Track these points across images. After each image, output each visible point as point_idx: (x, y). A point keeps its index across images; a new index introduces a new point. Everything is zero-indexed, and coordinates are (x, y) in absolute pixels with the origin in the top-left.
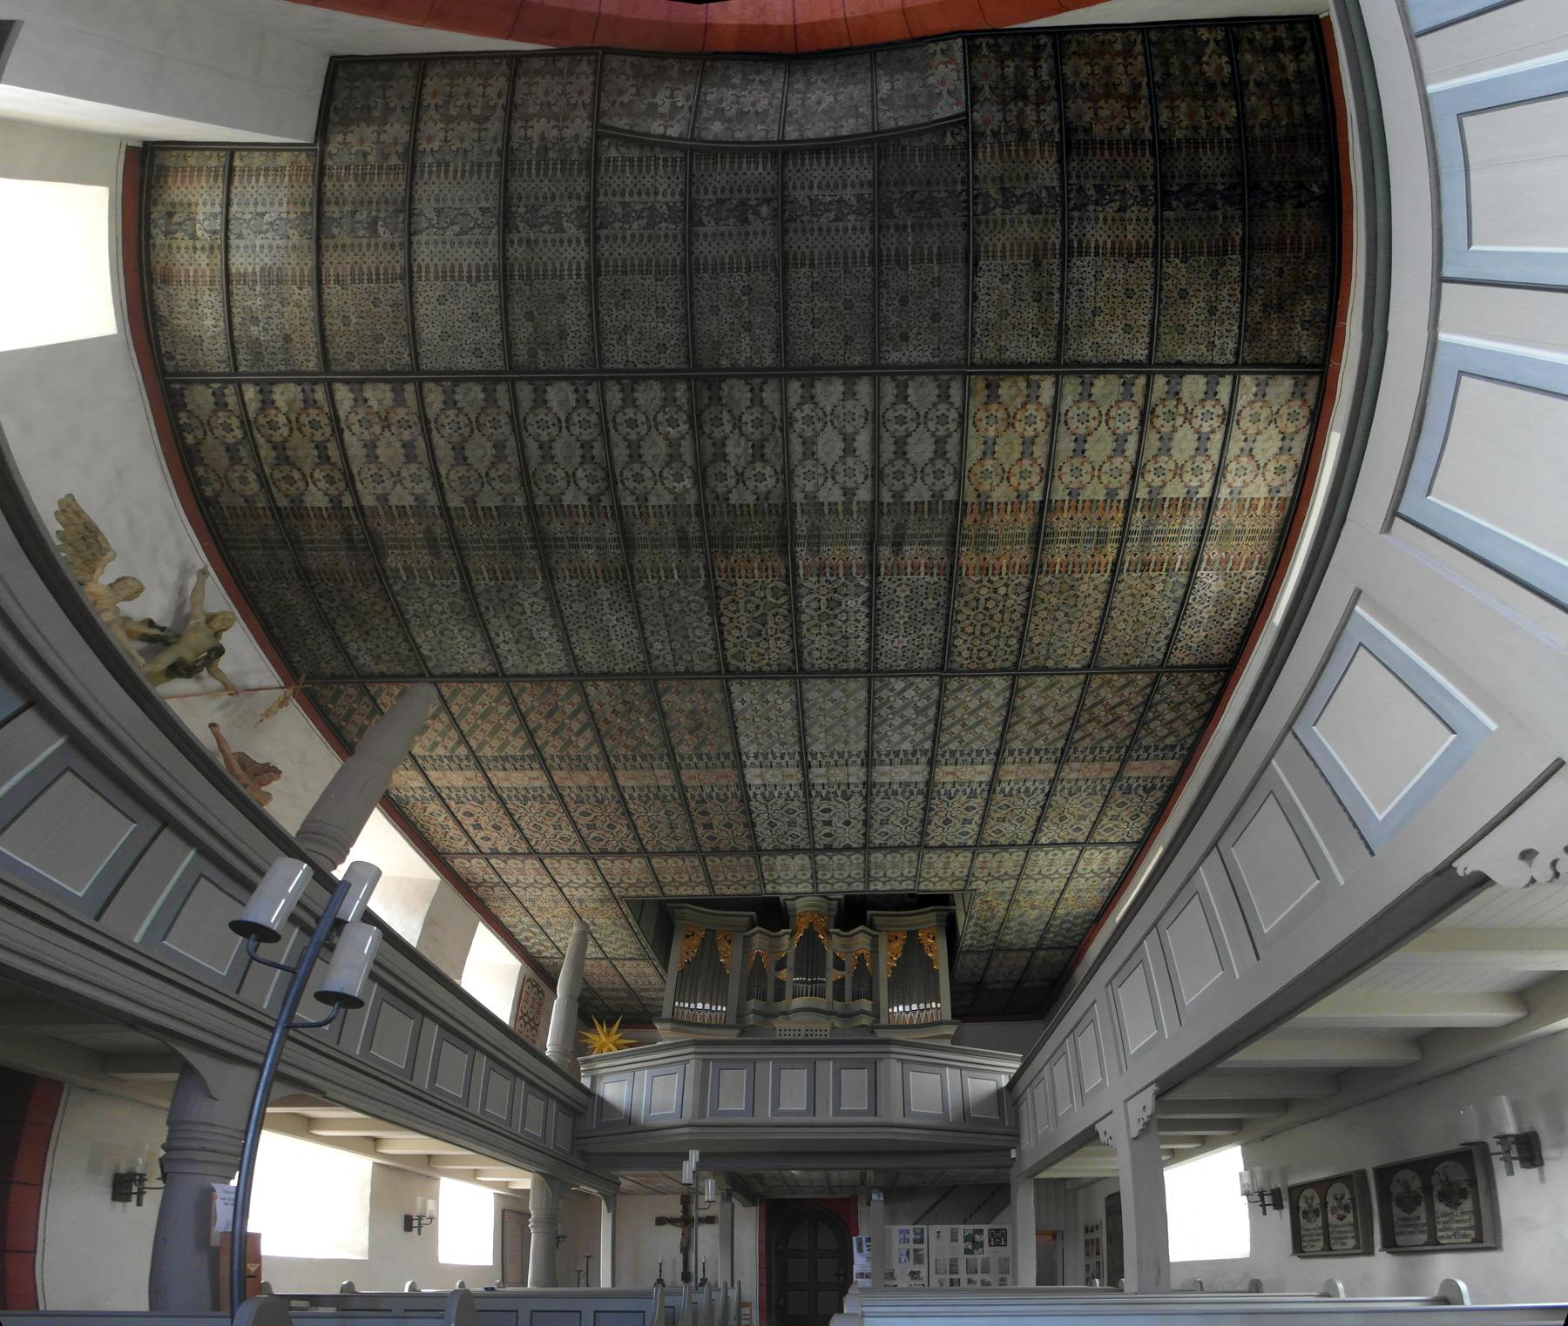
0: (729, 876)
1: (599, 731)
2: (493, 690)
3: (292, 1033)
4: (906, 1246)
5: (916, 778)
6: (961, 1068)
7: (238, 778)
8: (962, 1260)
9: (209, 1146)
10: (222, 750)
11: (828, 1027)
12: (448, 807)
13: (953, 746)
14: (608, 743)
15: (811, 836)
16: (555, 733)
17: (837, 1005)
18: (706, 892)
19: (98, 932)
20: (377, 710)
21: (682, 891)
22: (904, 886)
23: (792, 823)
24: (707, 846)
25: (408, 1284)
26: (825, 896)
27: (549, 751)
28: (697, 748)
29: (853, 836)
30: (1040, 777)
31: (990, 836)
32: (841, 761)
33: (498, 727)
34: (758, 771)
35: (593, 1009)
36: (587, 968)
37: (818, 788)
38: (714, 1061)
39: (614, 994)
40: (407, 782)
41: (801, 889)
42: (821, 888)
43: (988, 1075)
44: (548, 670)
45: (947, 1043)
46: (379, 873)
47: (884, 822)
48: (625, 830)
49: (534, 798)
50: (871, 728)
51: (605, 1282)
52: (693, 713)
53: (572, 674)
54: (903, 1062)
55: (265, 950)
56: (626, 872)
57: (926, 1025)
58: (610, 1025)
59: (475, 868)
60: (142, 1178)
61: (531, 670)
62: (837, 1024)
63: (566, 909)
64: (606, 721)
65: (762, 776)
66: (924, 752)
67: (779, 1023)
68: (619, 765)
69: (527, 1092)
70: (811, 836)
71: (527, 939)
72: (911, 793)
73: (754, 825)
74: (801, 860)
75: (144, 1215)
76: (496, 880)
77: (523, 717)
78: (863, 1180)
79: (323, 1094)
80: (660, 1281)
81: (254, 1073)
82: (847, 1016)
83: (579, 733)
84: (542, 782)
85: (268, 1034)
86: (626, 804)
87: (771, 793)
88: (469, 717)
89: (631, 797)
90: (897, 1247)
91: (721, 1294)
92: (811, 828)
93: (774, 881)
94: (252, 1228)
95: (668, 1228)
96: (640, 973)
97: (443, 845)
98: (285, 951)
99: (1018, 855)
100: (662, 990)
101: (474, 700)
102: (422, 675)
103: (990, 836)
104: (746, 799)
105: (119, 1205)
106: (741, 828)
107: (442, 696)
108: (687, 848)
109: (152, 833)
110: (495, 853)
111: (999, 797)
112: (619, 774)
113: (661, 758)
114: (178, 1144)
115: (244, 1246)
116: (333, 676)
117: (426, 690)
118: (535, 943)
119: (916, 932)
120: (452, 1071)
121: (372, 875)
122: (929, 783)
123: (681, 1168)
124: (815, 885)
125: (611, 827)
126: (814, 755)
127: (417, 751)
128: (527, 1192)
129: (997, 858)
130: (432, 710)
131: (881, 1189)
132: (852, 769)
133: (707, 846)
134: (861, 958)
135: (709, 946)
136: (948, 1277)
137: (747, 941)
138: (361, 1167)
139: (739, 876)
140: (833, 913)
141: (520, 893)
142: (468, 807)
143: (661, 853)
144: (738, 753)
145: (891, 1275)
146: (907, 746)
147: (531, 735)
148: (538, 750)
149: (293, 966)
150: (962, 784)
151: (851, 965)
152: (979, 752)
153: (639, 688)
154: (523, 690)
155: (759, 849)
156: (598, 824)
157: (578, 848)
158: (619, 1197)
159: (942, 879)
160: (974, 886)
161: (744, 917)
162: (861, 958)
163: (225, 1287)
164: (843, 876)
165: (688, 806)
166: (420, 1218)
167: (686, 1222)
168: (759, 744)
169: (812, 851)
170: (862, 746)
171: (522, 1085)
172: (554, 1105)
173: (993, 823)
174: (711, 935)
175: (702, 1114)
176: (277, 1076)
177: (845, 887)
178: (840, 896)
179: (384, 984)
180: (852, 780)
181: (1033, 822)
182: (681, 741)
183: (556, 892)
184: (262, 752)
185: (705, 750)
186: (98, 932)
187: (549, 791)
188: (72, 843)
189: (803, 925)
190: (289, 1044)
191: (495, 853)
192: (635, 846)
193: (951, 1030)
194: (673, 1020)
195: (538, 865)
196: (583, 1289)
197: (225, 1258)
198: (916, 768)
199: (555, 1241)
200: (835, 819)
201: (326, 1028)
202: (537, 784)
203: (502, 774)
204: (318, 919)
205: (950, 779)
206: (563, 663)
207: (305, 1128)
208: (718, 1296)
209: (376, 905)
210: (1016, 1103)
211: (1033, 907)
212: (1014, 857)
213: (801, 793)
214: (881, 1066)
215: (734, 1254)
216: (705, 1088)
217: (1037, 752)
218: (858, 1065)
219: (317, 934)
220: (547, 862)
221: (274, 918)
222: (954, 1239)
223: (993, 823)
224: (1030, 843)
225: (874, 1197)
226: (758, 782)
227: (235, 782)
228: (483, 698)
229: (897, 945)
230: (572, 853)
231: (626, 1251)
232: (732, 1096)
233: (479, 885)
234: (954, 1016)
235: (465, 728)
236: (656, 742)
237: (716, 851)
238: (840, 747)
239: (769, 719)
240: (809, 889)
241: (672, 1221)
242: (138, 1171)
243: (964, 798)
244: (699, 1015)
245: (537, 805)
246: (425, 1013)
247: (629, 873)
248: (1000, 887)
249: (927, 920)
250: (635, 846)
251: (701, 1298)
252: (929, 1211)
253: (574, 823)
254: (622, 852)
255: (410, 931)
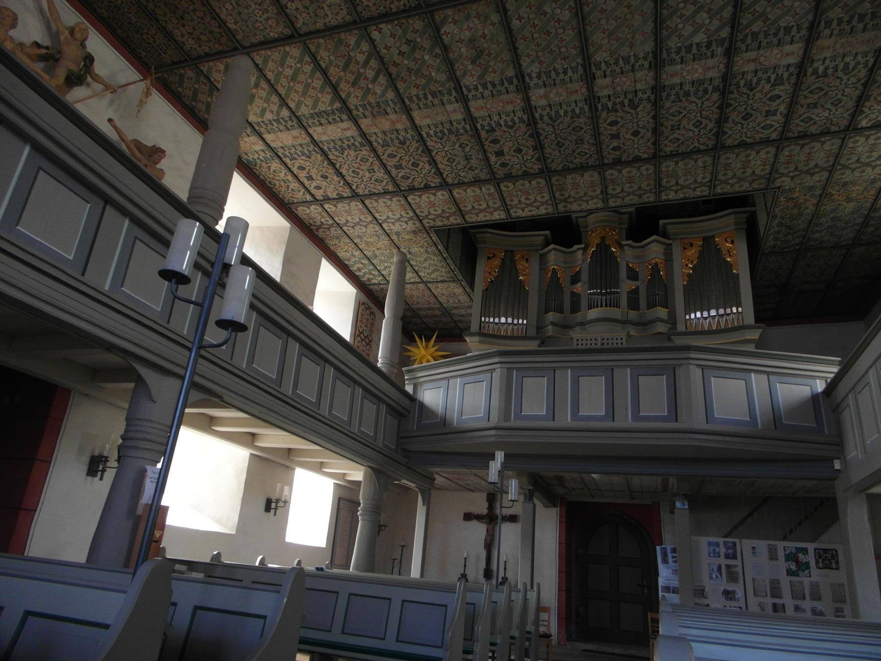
0: (523, 199)
1: (390, 75)
2: (294, 51)
3: (202, 352)
4: (716, 561)
5: (710, 74)
6: (768, 374)
7: (139, 160)
8: (785, 582)
9: (148, 437)
10: (123, 140)
11: (624, 335)
12: (285, 164)
13: (755, 28)
14: (401, 86)
15: (599, 151)
16: (354, 84)
17: (633, 315)
18: (503, 216)
19: (85, 284)
20: (213, 88)
21: (482, 217)
22: (698, 193)
23: (580, 141)
24: (501, 173)
25: (260, 558)
26: (614, 210)
27: (353, 102)
28: (481, 77)
29: (642, 147)
30: (864, 48)
31: (798, 126)
32: (628, 67)
33: (307, 86)
34: (542, 91)
35: (415, 326)
36: (407, 291)
37: (604, 100)
38: (518, 369)
39: (430, 312)
40: (251, 147)
41: (591, 205)
42: (612, 203)
43: (803, 379)
44: (334, 22)
45: (751, 348)
46: (247, 225)
47: (676, 127)
48: (427, 167)
49: (349, 147)
50: (659, 22)
51: (415, 572)
52: (472, 40)
53: (355, 22)
54: (703, 368)
55: (182, 290)
56: (432, 204)
57: (727, 330)
58: (428, 340)
59: (312, 213)
60: (106, 459)
61: (320, 25)
62: (632, 333)
63: (387, 242)
64: (396, 65)
65: (546, 96)
66: (721, 42)
67: (576, 334)
68: (413, 106)
69: (363, 398)
70: (599, 151)
71: (359, 270)
72: (706, 91)
73: (542, 147)
74: (590, 177)
75: (102, 486)
76: (331, 222)
77: (324, 73)
78: (665, 486)
79: (221, 398)
80: (464, 576)
81: (178, 382)
82: (643, 324)
83: (374, 80)
84: (352, 132)
85: (187, 353)
86: (424, 142)
87: (557, 113)
88: (283, 81)
89: (428, 134)
90: (706, 562)
91: (520, 596)
92: (598, 143)
93: (565, 200)
94: (164, 502)
95: (474, 523)
96: (451, 293)
97: (288, 196)
98: (194, 290)
99: (832, 144)
100: (470, 307)
101: (282, 65)
102: (236, 49)
103: (798, 126)
104: (532, 122)
105: (90, 478)
106: (531, 152)
107: (257, 65)
108: (483, 177)
109: (100, 210)
110: (327, 199)
111: (810, 79)
112: (415, 114)
113: (450, 94)
114: (130, 435)
115: (158, 512)
116: (173, 63)
117: (242, 62)
118: (365, 272)
119: (713, 237)
120: (309, 380)
121: (240, 226)
122: (727, 77)
123: (487, 467)
124: (605, 200)
125: (415, 165)
126: (598, 65)
127: (252, 118)
128: (358, 483)
129: (807, 150)
130: (253, 80)
131: (686, 497)
132: (639, 75)
133: (501, 173)
134: (655, 268)
135: (509, 266)
136: (770, 601)
137: (543, 258)
138: (240, 455)
139: (532, 198)
140: (625, 226)
141: (350, 232)
142: (300, 162)
143: (461, 184)
144: (521, 75)
145: (701, 592)
146: (701, 37)
147: (335, 88)
148: (344, 102)
149: (200, 301)
150: (765, 71)
151: (645, 274)
152: (788, 30)
153: (418, 24)
154: (318, 46)
155: (549, 170)
156: (404, 163)
157: (390, 188)
158: (433, 492)
159: (740, 180)
160: (778, 183)
161: (539, 237)
162: (655, 268)
163: (136, 549)
164: (633, 188)
165: (479, 136)
166: (277, 501)
167: (491, 519)
168: (541, 63)
169: (601, 167)
170: (649, 46)
171: (359, 391)
172: (384, 408)
173: (801, 111)
174: (510, 254)
175: (507, 417)
176: (194, 385)
177: (635, 200)
178: (632, 209)
179: (260, 313)
180: (639, 86)
181: (851, 104)
182: (465, 74)
183: (378, 228)
184: (150, 138)
185: (489, 78)
186: (85, 284)
187: (359, 139)
188: (57, 222)
189: (594, 239)
190: (201, 360)
191: (327, 199)
192: (438, 181)
193: (755, 335)
194: (480, 334)
195: (361, 206)
196: (395, 577)
197: (142, 525)
198: (711, 62)
199: (377, 528)
200: (623, 132)
201: (224, 347)
202: (349, 134)
203: (319, 129)
204: (212, 265)
205: (751, 67)
206: (344, 12)
207: (207, 425)
208: (517, 597)
209: (249, 250)
210: (836, 410)
211: (849, 200)
212: (827, 146)
213: (586, 109)
214: (680, 372)
215: (534, 557)
216: (510, 395)
217: (861, 18)
218: (657, 371)
219: (213, 276)
220: (367, 202)
221: (184, 265)
222: (773, 556)
223: (801, 111)
224: (847, 128)
225: (678, 505)
226: (543, 102)
227: (138, 163)
228: (289, 61)
229: (693, 252)
230: (386, 192)
231: (438, 546)
232: (534, 402)
233: (319, 227)
234: (758, 319)
235: (282, 91)
236: (442, 77)
237: (509, 177)
238: (625, 51)
239: (548, 33)
240: (600, 205)
241: (479, 518)
242: (105, 454)
243: (767, 87)
244: (503, 329)
245: (352, 153)
246: (289, 334)
247: (435, 205)
248: (809, 181)
249: (725, 230)
250: (438, 181)
251: (501, 597)
252: (741, 523)
253: (384, 165)
254: (427, 187)
255: (274, 268)
